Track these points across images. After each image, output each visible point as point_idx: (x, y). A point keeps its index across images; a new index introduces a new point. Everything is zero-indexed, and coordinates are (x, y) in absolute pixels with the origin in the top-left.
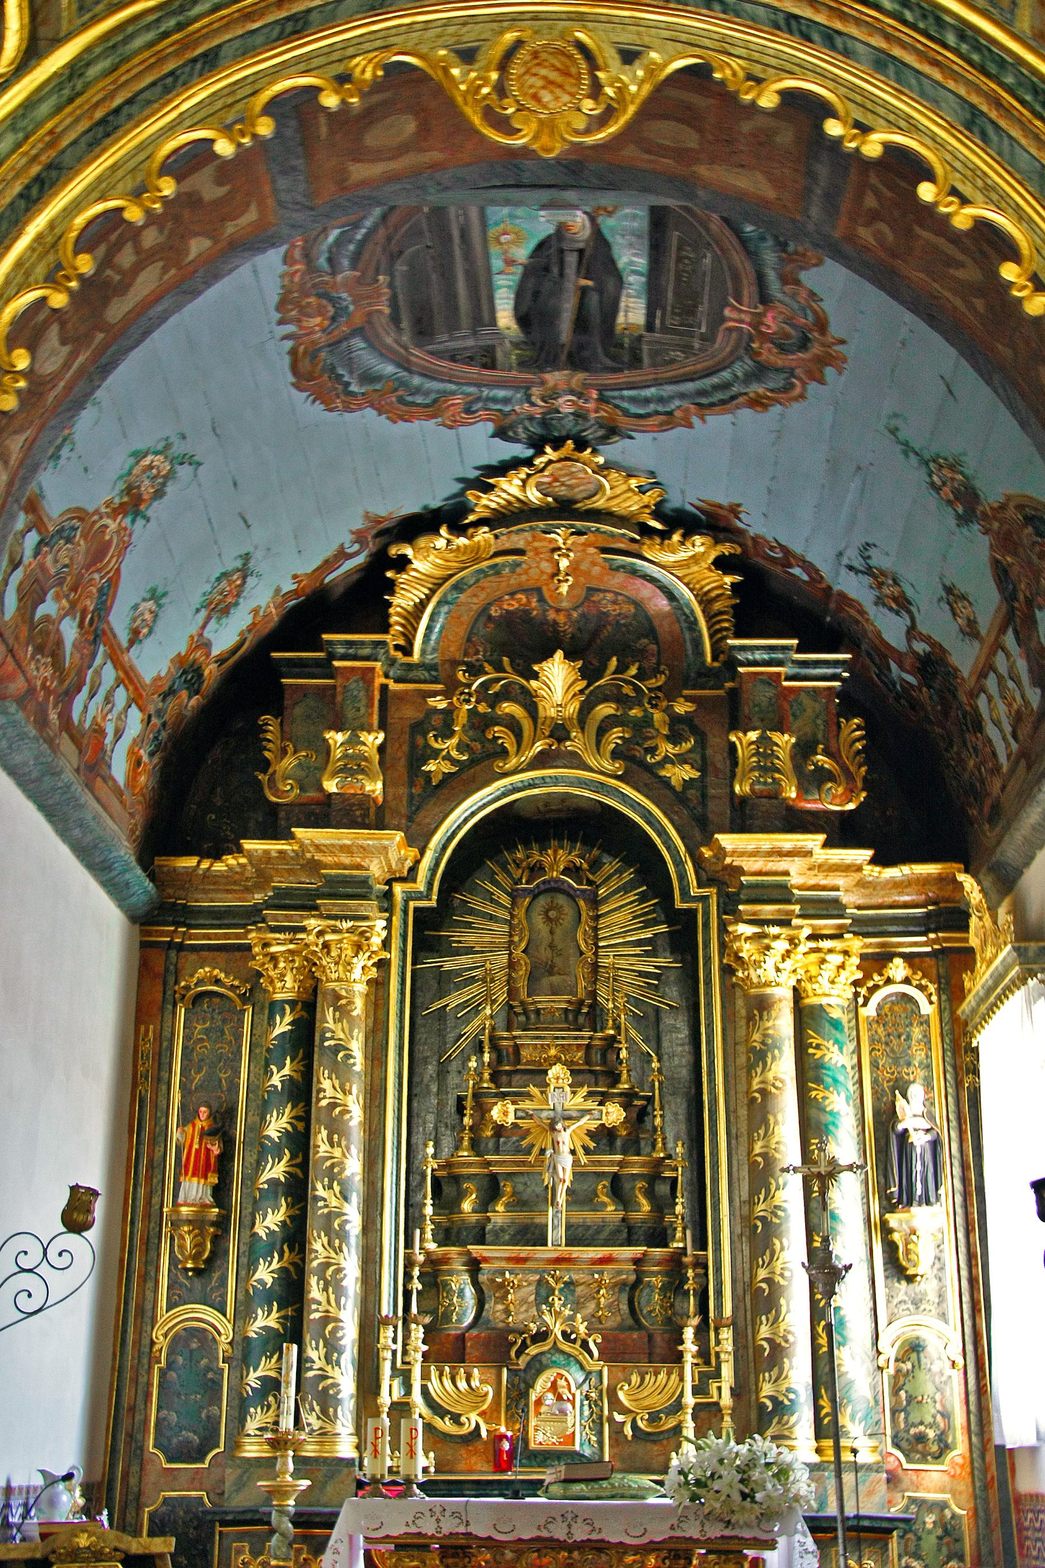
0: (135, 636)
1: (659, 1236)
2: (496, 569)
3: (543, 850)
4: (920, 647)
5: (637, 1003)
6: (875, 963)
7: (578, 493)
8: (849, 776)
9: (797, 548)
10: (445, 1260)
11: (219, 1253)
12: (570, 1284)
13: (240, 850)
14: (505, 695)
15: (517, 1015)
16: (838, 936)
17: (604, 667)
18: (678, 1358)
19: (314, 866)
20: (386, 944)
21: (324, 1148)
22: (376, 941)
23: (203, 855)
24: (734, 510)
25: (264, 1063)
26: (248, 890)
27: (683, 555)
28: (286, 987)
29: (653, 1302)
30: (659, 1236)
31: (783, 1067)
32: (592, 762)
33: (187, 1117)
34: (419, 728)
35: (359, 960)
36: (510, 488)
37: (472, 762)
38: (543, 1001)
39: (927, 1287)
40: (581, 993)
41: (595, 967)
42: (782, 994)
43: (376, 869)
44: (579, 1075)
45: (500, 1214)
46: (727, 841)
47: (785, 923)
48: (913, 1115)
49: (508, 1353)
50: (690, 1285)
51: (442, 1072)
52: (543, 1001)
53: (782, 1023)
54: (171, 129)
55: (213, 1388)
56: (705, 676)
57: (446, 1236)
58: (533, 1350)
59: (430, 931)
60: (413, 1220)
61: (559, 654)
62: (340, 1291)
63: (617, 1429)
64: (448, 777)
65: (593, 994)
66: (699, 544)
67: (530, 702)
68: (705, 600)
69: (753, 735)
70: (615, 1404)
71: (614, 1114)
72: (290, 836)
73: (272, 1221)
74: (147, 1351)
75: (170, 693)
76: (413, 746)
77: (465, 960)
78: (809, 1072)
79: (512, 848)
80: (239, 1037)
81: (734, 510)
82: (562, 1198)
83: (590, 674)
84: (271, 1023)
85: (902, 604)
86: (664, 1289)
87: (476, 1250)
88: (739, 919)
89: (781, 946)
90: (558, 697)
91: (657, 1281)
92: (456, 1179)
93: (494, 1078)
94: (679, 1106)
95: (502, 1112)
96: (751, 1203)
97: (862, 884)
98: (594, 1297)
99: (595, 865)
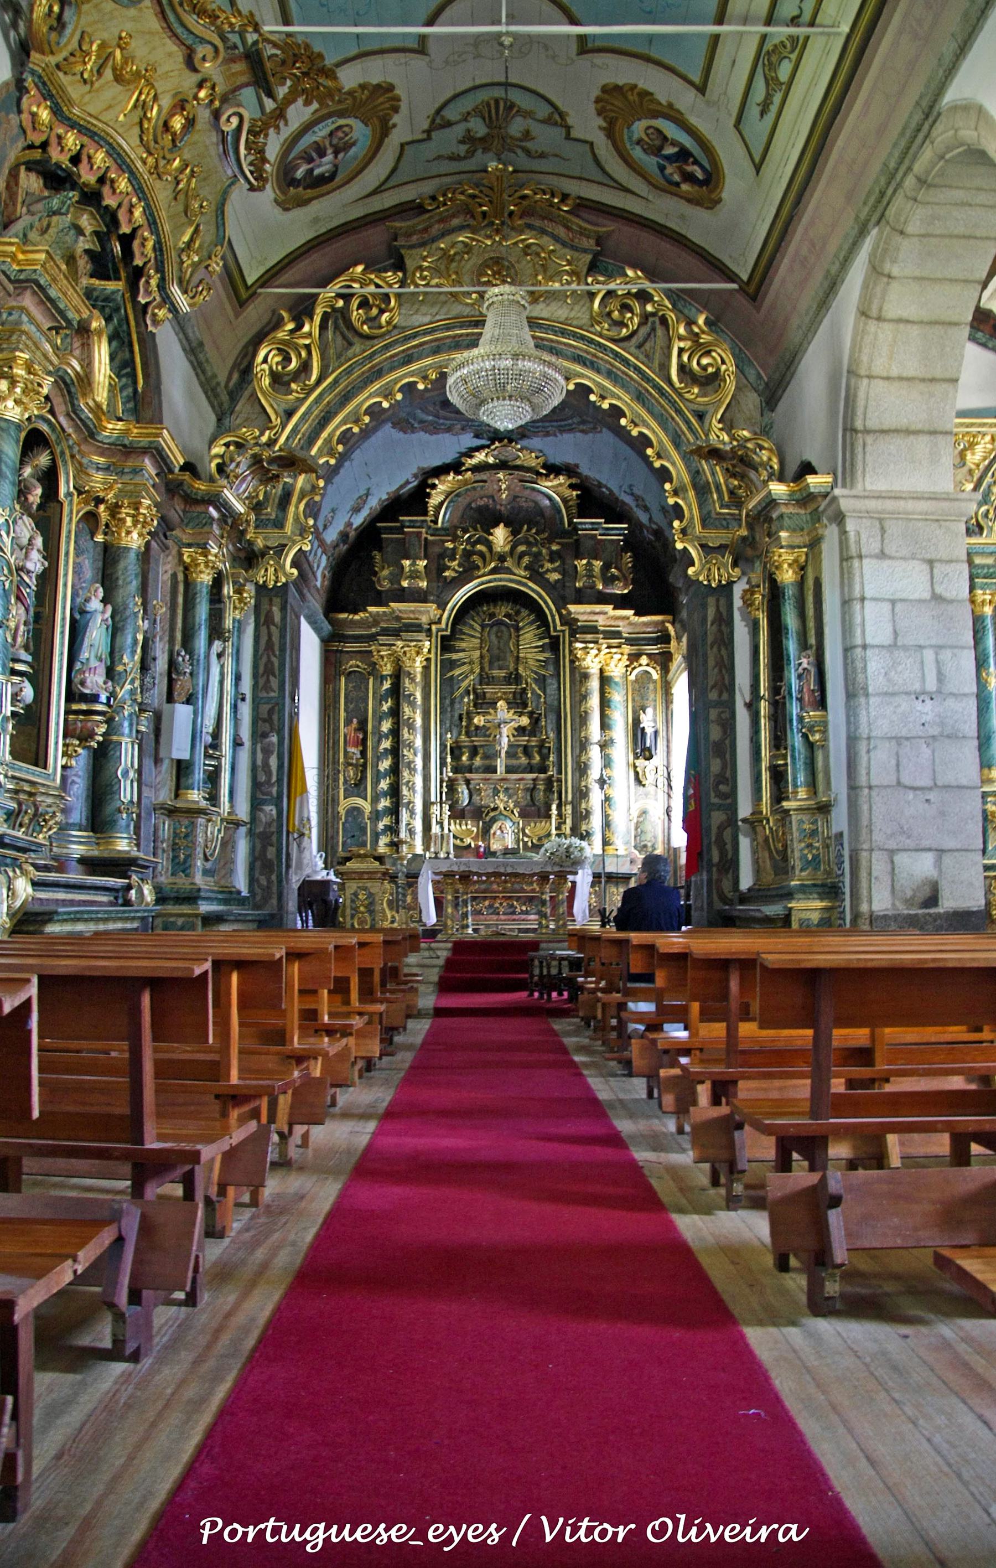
0: (325, 527)
1: (543, 769)
2: (474, 488)
3: (495, 606)
4: (654, 527)
5: (536, 673)
6: (634, 657)
7: (510, 458)
8: (626, 579)
9: (604, 482)
10: (456, 780)
11: (364, 778)
12: (507, 789)
13: (366, 611)
14: (478, 541)
15: (485, 679)
16: (619, 647)
17: (521, 528)
18: (549, 817)
19: (398, 619)
20: (429, 651)
21: (406, 736)
22: (426, 650)
23: (350, 612)
24: (577, 466)
25: (380, 699)
26: (370, 627)
27: (556, 482)
28: (387, 669)
29: (540, 796)
30: (543, 769)
31: (594, 702)
32: (516, 571)
33: (348, 722)
34: (441, 556)
35: (419, 657)
36: (480, 457)
37: (464, 571)
38: (495, 672)
39: (650, 788)
40: (511, 668)
41: (518, 657)
42: (594, 671)
43: (424, 619)
44: (510, 705)
45: (478, 761)
46: (572, 608)
47: (596, 642)
48: (647, 721)
49: (483, 816)
50: (555, 789)
51: (452, 702)
52: (495, 672)
53: (594, 684)
54: (367, 398)
55: (363, 830)
56: (564, 534)
57: (456, 770)
58: (492, 814)
59: (447, 644)
60: (443, 764)
61: (502, 525)
62: (414, 792)
63: (525, 843)
64: (454, 578)
65: (517, 669)
66: (562, 479)
67: (489, 545)
68: (565, 501)
69: (584, 562)
70: (524, 834)
71: (525, 721)
72: (387, 605)
73: (385, 764)
74: (336, 816)
75: (337, 545)
76: (439, 564)
77: (461, 655)
78: (605, 703)
79: (481, 605)
80: (367, 689)
81: (577, 466)
82: (503, 755)
83: (514, 533)
84: (382, 684)
85: (646, 509)
86: (545, 791)
87: (468, 775)
88: (577, 641)
89: (594, 652)
90: (501, 543)
91: (542, 787)
92: (460, 748)
93: (475, 705)
94: (552, 717)
95: (478, 720)
96: (580, 756)
97: (630, 624)
98: (516, 794)
99: (518, 613)
